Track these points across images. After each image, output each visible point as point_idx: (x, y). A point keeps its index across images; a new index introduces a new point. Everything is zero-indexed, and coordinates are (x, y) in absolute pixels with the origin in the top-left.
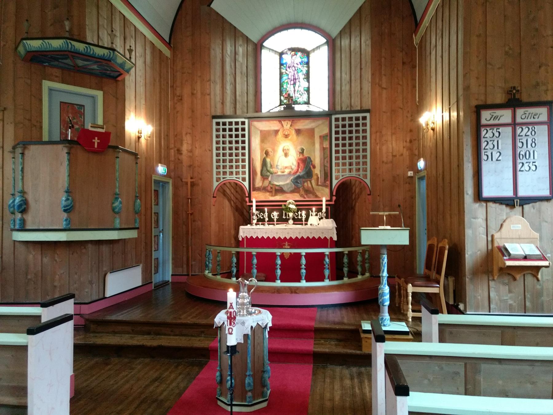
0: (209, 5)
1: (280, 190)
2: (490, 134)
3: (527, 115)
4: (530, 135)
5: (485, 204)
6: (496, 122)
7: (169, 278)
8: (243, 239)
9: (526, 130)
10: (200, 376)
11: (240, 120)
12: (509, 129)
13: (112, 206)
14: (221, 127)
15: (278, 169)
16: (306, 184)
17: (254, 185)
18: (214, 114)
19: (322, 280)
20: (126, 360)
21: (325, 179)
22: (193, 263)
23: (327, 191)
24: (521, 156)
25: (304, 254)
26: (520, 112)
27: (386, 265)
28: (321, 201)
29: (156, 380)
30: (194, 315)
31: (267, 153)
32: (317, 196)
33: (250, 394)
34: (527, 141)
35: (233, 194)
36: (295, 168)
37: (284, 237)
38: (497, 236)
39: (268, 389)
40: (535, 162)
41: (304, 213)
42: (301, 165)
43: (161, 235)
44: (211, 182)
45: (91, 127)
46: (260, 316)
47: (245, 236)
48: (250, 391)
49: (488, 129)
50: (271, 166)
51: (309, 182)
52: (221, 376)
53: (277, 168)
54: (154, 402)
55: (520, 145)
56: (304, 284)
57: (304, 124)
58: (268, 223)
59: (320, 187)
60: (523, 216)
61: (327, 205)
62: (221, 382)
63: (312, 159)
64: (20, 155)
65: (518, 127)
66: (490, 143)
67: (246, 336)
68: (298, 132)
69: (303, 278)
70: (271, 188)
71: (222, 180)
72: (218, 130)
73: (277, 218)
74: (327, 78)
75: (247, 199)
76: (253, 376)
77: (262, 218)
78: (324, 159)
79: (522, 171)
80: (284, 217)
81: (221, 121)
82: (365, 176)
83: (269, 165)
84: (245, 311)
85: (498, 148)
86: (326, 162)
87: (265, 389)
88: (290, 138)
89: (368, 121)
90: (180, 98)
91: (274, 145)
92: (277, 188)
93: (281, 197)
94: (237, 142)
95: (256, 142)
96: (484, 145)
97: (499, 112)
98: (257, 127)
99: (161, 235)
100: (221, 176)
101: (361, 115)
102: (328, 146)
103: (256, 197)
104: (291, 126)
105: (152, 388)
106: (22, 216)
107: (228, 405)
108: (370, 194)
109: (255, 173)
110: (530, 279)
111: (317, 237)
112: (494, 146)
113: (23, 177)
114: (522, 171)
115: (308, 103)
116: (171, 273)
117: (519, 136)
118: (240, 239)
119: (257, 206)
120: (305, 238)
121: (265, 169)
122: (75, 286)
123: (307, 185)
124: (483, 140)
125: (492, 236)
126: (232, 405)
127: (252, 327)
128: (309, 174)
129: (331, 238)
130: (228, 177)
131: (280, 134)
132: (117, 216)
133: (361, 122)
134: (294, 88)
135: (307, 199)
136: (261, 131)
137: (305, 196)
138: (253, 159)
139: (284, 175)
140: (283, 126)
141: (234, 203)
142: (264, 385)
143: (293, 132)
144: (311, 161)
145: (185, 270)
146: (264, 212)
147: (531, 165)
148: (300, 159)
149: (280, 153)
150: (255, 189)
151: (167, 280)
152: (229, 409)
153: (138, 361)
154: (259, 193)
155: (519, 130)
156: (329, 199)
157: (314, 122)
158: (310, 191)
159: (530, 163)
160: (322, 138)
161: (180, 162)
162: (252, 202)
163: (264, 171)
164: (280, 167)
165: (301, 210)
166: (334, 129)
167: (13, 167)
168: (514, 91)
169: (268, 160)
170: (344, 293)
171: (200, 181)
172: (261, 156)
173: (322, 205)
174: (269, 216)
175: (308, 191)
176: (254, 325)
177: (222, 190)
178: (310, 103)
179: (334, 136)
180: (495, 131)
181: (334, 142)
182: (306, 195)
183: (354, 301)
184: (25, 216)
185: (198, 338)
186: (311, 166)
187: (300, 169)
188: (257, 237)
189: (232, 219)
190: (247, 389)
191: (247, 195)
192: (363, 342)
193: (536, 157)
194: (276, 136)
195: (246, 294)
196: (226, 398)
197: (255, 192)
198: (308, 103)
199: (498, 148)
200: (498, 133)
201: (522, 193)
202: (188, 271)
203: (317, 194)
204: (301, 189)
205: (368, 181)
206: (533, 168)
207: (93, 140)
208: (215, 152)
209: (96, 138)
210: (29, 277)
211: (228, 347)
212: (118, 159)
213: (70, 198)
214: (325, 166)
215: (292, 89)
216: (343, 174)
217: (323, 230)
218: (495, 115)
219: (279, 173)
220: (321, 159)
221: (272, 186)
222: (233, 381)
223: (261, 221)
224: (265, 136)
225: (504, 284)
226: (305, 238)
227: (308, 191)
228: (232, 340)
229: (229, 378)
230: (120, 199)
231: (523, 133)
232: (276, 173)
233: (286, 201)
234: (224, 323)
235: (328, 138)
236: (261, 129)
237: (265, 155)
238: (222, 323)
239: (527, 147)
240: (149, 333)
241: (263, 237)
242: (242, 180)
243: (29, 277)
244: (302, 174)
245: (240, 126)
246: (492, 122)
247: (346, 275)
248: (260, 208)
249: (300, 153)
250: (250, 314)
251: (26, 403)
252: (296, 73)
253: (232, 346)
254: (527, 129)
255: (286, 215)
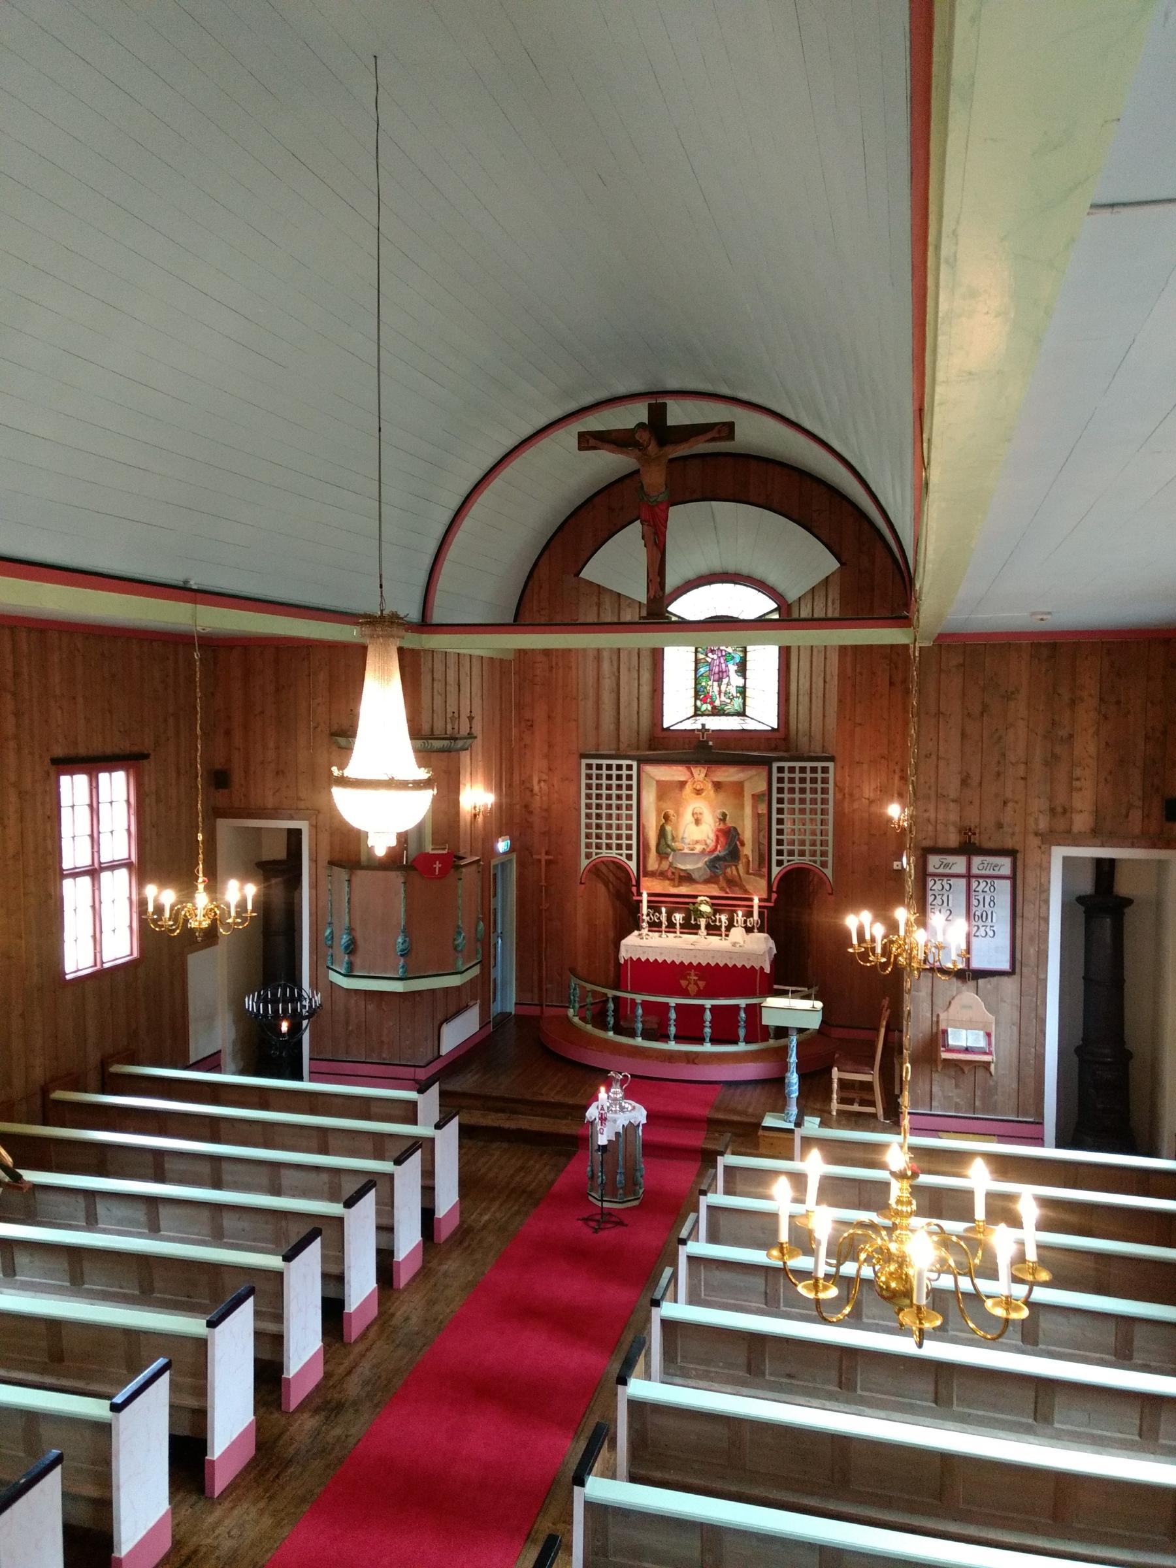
0: (577, 574)
1: (687, 878)
2: (938, 886)
3: (985, 865)
4: (989, 891)
5: (931, 975)
6: (947, 871)
7: (511, 1008)
8: (626, 961)
9: (983, 884)
10: (568, 1168)
11: (624, 762)
12: (963, 881)
13: (453, 944)
14: (594, 772)
15: (685, 844)
16: (729, 870)
17: (645, 867)
18: (582, 751)
19: (735, 1042)
20: (481, 1144)
21: (759, 864)
22: (549, 986)
23: (763, 883)
24: (977, 917)
25: (709, 1007)
26: (977, 861)
27: (795, 1049)
28: (751, 900)
29: (521, 1169)
30: (558, 1089)
31: (667, 817)
32: (746, 891)
33: (621, 1191)
34: (984, 898)
35: (613, 874)
36: (711, 843)
37: (689, 962)
38: (943, 1016)
39: (640, 1188)
40: (993, 926)
41: (724, 918)
42: (722, 839)
43: (500, 941)
44: (578, 864)
45: (433, 849)
46: (634, 1113)
47: (629, 956)
48: (621, 1188)
49: (936, 879)
50: (673, 838)
51: (734, 868)
52: (592, 1171)
53: (683, 842)
54: (524, 1191)
55: (975, 902)
56: (708, 1047)
57: (726, 774)
58: (667, 930)
59: (752, 876)
60: (977, 994)
61: (760, 907)
62: (593, 1177)
63: (739, 830)
64: (346, 883)
65: (974, 880)
66: (939, 897)
67: (617, 1134)
68: (718, 786)
69: (708, 1040)
70: (673, 873)
71: (594, 857)
72: (589, 777)
73: (681, 922)
74: (777, 672)
75: (634, 889)
76: (625, 1174)
77: (657, 921)
78: (760, 831)
79: (978, 936)
80: (693, 922)
81: (594, 762)
82: (824, 864)
83: (670, 837)
84: (618, 1106)
85: (948, 905)
86: (761, 837)
87: (638, 1188)
88: (703, 794)
89: (831, 775)
90: (529, 723)
91: (678, 806)
92: (682, 874)
93: (689, 889)
94: (619, 787)
95: (649, 798)
96: (930, 899)
97: (950, 859)
98: (652, 775)
99: (500, 941)
100: (594, 850)
101: (819, 765)
102: (765, 811)
103: (649, 887)
104: (706, 776)
105: (517, 1179)
106: (349, 957)
107: (599, 1200)
108: (832, 894)
109: (647, 847)
110: (980, 1073)
111: (739, 966)
112: (943, 902)
113: (349, 909)
114: (978, 936)
115: (742, 713)
116: (514, 1001)
117: (975, 891)
118: (622, 961)
119: (649, 902)
120: (721, 965)
121: (663, 842)
122: (407, 1042)
123: (731, 871)
124: (930, 893)
125: (938, 1016)
126: (602, 1201)
127: (623, 1126)
128: (734, 854)
129: (762, 969)
130: (604, 852)
131: (688, 788)
132: (460, 955)
133: (819, 775)
134: (719, 686)
135: (730, 895)
136: (658, 782)
137: (728, 890)
138: (643, 825)
139: (694, 854)
140: (692, 774)
141: (614, 886)
142: (636, 1184)
143: (710, 786)
144: (738, 834)
145: (536, 997)
146: (660, 913)
147: (988, 930)
148: (719, 830)
149: (688, 817)
150: (646, 874)
151: (508, 1011)
152: (599, 1204)
153: (494, 1145)
154: (652, 881)
155: (974, 884)
156: (765, 896)
157: (743, 771)
158: (736, 882)
159: (987, 926)
160: (756, 798)
161: (530, 825)
162: (640, 894)
163: (661, 846)
164: (687, 841)
165: (721, 912)
166: (775, 785)
167: (330, 887)
168: (970, 834)
169: (668, 828)
170: (761, 1064)
171: (560, 857)
172: (658, 822)
173: (752, 907)
174: (669, 919)
175: (731, 883)
176: (626, 1123)
177: (596, 870)
178: (747, 714)
179: (775, 796)
180: (944, 883)
181: (775, 806)
182: (730, 888)
183: (777, 1076)
184: (352, 958)
185: (564, 1122)
186: (738, 843)
187: (719, 846)
188: (648, 960)
189: (611, 912)
190: (619, 1186)
191: (634, 883)
192: (761, 1141)
193: (994, 921)
194: (681, 791)
195: (619, 1090)
196: (597, 1192)
197: (646, 878)
198: (742, 713)
199: (948, 905)
200: (948, 886)
201: (976, 964)
202: (540, 998)
203: (748, 887)
204: (721, 878)
205: (829, 872)
206: (991, 934)
207: (434, 866)
208: (583, 811)
209: (437, 862)
210: (350, 1028)
211: (599, 1146)
212: (460, 882)
213: (407, 939)
214: (760, 843)
215: (716, 689)
216: (790, 858)
217: (749, 955)
218: (945, 862)
219: (686, 851)
220: (753, 832)
221: (674, 871)
222: (604, 1177)
223: (655, 926)
224: (665, 790)
225: (950, 1077)
226: (721, 965)
227: (731, 883)
228: (602, 1140)
229: (600, 1174)
230: (463, 934)
231: (980, 889)
232: (681, 850)
233: (696, 897)
234: (595, 1119)
235: (766, 798)
236: (657, 778)
237: (663, 821)
238: (593, 1118)
239: (984, 906)
240: (503, 1111)
241: (656, 960)
242: (627, 858)
243: (350, 1028)
244: (722, 854)
245: (624, 772)
246: (941, 871)
247: (772, 1035)
248: (654, 907)
249: (720, 820)
250: (622, 1109)
251: (434, 1184)
252: (722, 661)
253: (603, 1146)
254: (985, 883)
255: (695, 920)
